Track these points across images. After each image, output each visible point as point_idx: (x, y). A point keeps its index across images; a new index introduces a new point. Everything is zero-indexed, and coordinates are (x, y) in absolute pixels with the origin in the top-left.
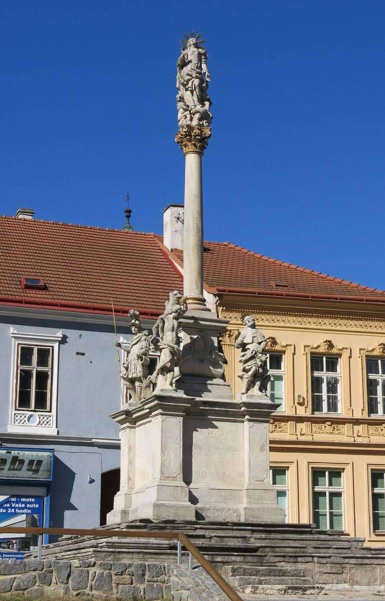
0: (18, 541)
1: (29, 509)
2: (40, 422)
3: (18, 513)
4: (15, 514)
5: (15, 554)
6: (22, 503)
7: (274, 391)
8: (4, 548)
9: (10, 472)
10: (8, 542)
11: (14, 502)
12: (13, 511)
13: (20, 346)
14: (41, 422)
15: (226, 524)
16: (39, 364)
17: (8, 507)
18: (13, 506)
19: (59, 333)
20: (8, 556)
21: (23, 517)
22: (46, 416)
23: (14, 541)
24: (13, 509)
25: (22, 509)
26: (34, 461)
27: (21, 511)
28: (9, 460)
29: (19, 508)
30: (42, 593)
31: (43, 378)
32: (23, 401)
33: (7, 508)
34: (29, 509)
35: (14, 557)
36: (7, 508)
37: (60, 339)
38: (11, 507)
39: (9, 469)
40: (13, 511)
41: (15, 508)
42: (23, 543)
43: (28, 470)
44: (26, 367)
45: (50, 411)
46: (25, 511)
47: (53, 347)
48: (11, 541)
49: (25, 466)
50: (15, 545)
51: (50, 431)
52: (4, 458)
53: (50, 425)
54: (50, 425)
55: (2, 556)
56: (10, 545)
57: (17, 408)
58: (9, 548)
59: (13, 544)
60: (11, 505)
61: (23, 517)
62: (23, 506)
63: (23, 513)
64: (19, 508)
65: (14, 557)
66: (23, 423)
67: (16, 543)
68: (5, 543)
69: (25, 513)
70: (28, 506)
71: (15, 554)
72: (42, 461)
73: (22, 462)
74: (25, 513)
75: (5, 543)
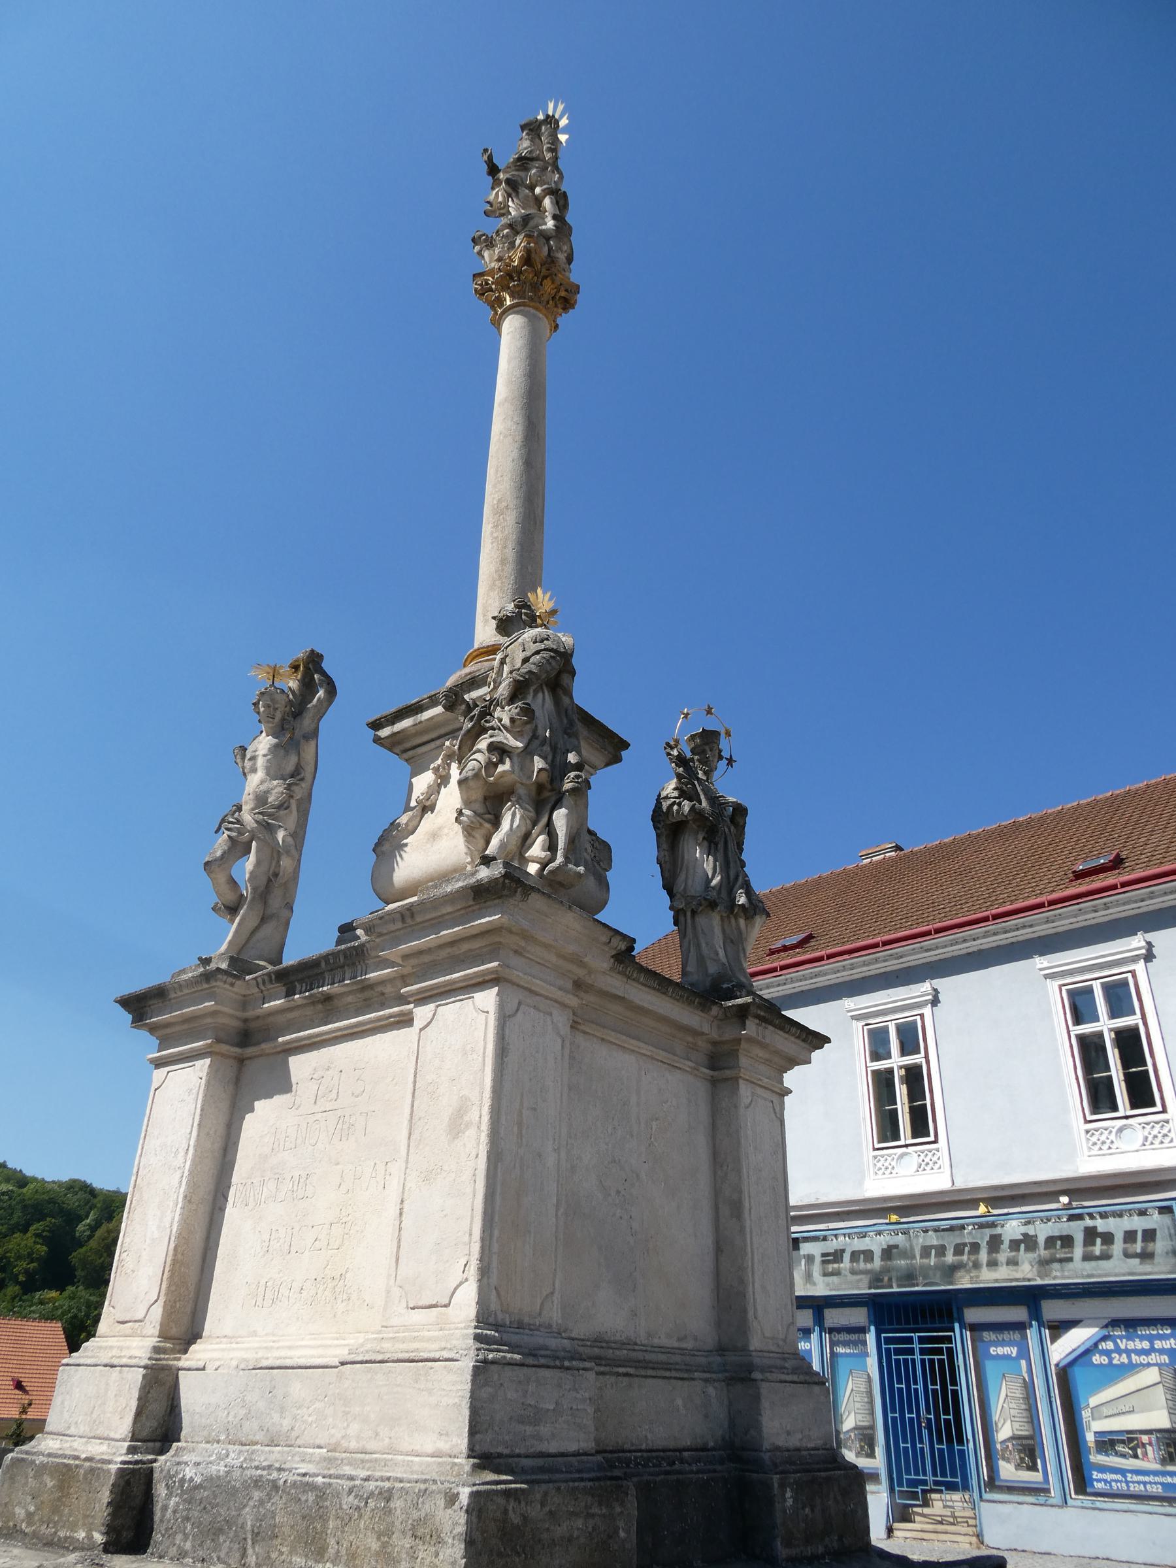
0: (1153, 1438)
1: (1162, 1351)
2: (1146, 1139)
3: (1137, 1365)
4: (1130, 1369)
5: (1155, 1473)
6: (1142, 1338)
7: (1081, 1039)
8: (1124, 1456)
9: (1089, 1266)
10: (1131, 1440)
11: (1121, 1337)
12: (1124, 1359)
13: (1064, 988)
14: (1150, 1138)
15: (1029, 1410)
16: (904, 1053)
17: (1111, 1351)
18: (1123, 1347)
19: (1137, 942)
20: (1141, 1478)
21: (1151, 1375)
22: (1157, 1123)
23: (1145, 1439)
24: (1124, 1355)
25: (1146, 1352)
26: (1135, 1232)
27: (1144, 1359)
28: (1079, 1238)
29: (1140, 1352)
30: (291, 1562)
31: (1130, 1043)
32: (888, 1129)
33: (1107, 1353)
34: (1162, 1351)
35: (1155, 1483)
36: (1107, 1353)
37: (930, 997)
38: (1119, 1351)
39: (1087, 1257)
40: (1126, 1361)
41: (1128, 1352)
42: (1168, 1445)
43: (1127, 1255)
44: (1086, 1028)
45: (936, 1142)
46: (1153, 1358)
47: (1133, 973)
48: (1136, 1439)
49: (1118, 1247)
50: (1149, 1448)
51: (936, 1182)
52: (1065, 1233)
53: (1171, 1141)
54: (1171, 1141)
55: (1125, 1477)
56: (1137, 1446)
57: (932, 1138)
58: (1136, 1456)
59: (1144, 1445)
60: (1116, 1344)
61: (1151, 1375)
62: (1146, 1345)
63: (1149, 1365)
64: (1140, 1352)
65: (1155, 1483)
66: (1162, 1142)
67: (1150, 1444)
68: (1123, 1442)
69: (1154, 1365)
70: (1158, 1344)
71: (1155, 1473)
72: (1155, 1230)
73: (1108, 1238)
74: (1154, 1365)
75: (1123, 1442)
